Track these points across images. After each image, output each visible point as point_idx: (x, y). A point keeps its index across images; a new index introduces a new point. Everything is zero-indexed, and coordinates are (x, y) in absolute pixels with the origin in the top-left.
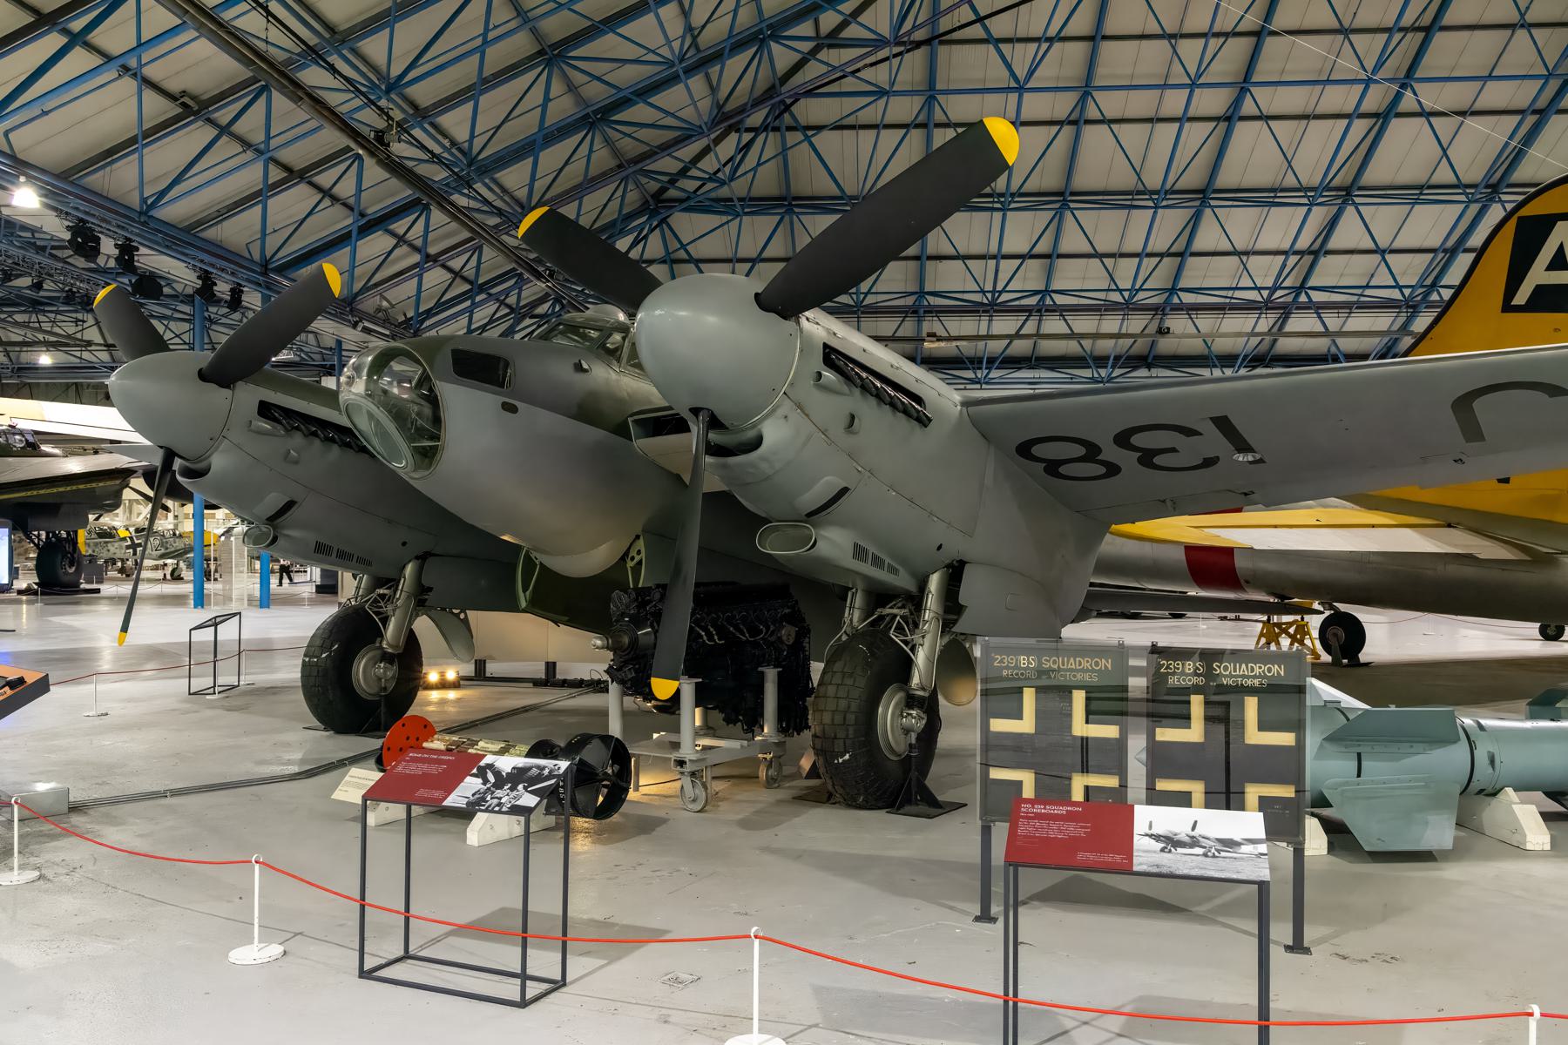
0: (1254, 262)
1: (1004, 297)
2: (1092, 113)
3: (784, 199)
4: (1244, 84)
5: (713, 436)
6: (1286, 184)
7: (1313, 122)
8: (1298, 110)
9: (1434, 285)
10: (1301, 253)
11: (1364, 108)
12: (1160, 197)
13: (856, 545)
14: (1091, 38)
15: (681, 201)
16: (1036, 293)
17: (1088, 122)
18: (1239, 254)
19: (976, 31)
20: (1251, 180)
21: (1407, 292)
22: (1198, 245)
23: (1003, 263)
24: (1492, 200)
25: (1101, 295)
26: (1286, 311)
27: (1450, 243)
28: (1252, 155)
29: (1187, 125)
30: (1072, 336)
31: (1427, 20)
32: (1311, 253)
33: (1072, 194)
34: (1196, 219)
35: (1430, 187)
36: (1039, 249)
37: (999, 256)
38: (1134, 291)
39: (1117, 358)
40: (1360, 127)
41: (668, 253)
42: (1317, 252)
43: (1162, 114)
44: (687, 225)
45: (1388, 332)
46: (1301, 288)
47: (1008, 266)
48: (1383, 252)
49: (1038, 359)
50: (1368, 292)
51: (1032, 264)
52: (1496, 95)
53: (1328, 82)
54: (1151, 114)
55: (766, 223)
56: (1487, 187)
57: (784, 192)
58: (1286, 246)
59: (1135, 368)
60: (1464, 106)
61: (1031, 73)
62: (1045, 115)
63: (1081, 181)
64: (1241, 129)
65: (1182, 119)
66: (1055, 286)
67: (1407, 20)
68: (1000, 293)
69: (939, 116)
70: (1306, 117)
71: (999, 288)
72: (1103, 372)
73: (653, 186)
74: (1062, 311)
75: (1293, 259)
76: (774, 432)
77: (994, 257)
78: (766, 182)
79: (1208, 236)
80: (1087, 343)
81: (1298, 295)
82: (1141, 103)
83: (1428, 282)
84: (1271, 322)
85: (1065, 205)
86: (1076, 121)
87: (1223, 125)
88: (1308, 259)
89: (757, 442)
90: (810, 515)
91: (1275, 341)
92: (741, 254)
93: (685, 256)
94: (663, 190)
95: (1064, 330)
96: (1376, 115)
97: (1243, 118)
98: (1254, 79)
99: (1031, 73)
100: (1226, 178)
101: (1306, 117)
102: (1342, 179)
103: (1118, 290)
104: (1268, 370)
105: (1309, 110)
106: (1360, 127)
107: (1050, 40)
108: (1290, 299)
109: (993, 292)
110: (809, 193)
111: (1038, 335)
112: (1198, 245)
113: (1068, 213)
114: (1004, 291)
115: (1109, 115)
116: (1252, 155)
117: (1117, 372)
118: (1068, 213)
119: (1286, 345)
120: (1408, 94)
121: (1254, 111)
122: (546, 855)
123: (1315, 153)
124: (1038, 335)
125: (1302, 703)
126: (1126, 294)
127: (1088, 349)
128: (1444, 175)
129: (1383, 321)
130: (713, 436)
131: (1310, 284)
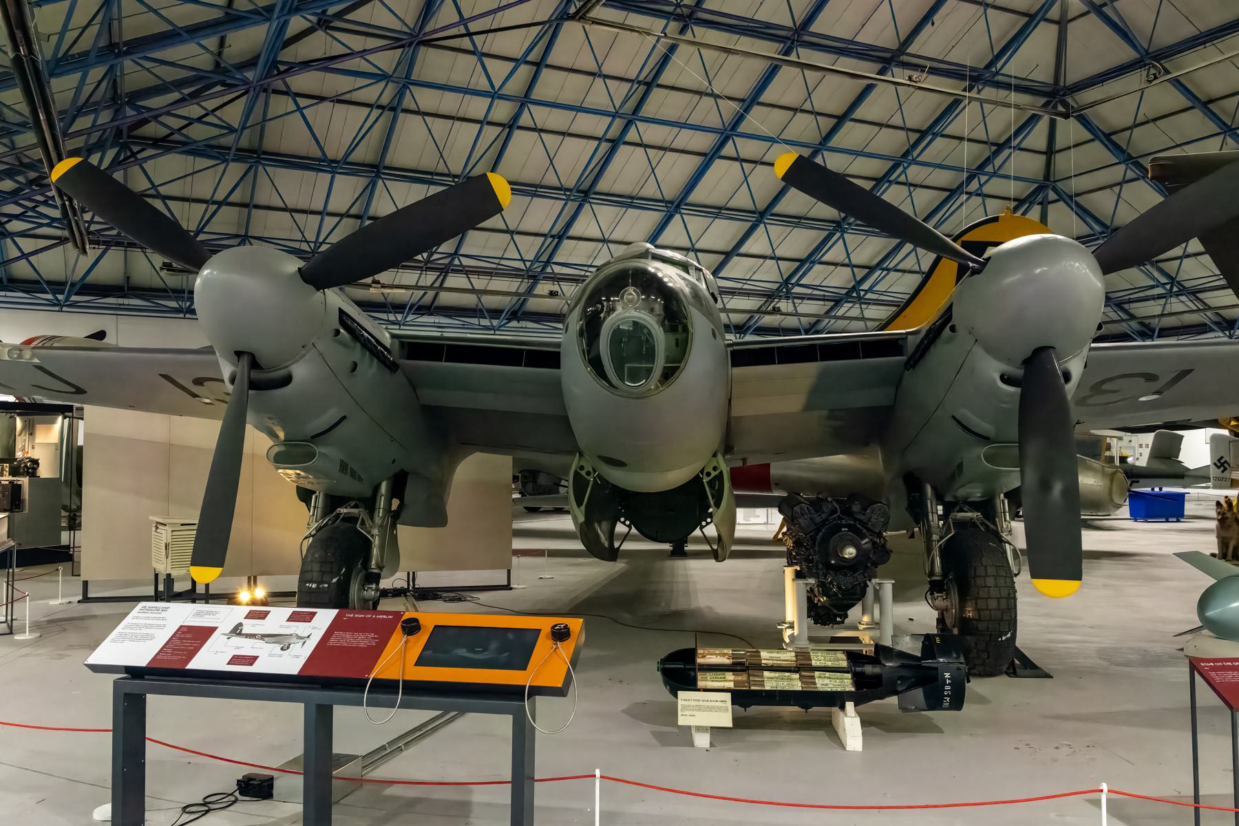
3: (254, 152)
4: (729, 132)
5: (255, 375)
7: (567, 139)
8: (659, 143)
13: (342, 461)
15: (184, 144)
18: (512, 233)
19: (466, 43)
20: (617, 189)
23: (327, 219)
24: (584, 201)
26: (535, 278)
29: (486, 127)
30: (473, 291)
31: (649, 79)
34: (372, 186)
35: (542, 187)
39: (412, 306)
40: (491, 133)
45: (516, 294)
47: (330, 222)
48: (512, 233)
50: (503, 262)
54: (564, 129)
60: (757, 158)
65: (484, 122)
67: (641, 78)
68: (321, 244)
70: (563, 134)
74: (467, 272)
76: (300, 371)
81: (453, 260)
82: (449, 102)
83: (544, 258)
85: (378, 176)
87: (388, 115)
89: (288, 380)
90: (313, 437)
91: (437, 294)
95: (791, 309)
97: (1050, 203)
101: (563, 134)
102: (585, 186)
104: (121, 301)
105: (667, 145)
106: (491, 133)
108: (446, 261)
109: (315, 243)
110: (275, 150)
113: (261, 168)
115: (646, 141)
118: (261, 168)
119: (446, 298)
120: (633, 128)
122: (704, 680)
128: (551, 180)
130: (255, 375)
131: (461, 252)
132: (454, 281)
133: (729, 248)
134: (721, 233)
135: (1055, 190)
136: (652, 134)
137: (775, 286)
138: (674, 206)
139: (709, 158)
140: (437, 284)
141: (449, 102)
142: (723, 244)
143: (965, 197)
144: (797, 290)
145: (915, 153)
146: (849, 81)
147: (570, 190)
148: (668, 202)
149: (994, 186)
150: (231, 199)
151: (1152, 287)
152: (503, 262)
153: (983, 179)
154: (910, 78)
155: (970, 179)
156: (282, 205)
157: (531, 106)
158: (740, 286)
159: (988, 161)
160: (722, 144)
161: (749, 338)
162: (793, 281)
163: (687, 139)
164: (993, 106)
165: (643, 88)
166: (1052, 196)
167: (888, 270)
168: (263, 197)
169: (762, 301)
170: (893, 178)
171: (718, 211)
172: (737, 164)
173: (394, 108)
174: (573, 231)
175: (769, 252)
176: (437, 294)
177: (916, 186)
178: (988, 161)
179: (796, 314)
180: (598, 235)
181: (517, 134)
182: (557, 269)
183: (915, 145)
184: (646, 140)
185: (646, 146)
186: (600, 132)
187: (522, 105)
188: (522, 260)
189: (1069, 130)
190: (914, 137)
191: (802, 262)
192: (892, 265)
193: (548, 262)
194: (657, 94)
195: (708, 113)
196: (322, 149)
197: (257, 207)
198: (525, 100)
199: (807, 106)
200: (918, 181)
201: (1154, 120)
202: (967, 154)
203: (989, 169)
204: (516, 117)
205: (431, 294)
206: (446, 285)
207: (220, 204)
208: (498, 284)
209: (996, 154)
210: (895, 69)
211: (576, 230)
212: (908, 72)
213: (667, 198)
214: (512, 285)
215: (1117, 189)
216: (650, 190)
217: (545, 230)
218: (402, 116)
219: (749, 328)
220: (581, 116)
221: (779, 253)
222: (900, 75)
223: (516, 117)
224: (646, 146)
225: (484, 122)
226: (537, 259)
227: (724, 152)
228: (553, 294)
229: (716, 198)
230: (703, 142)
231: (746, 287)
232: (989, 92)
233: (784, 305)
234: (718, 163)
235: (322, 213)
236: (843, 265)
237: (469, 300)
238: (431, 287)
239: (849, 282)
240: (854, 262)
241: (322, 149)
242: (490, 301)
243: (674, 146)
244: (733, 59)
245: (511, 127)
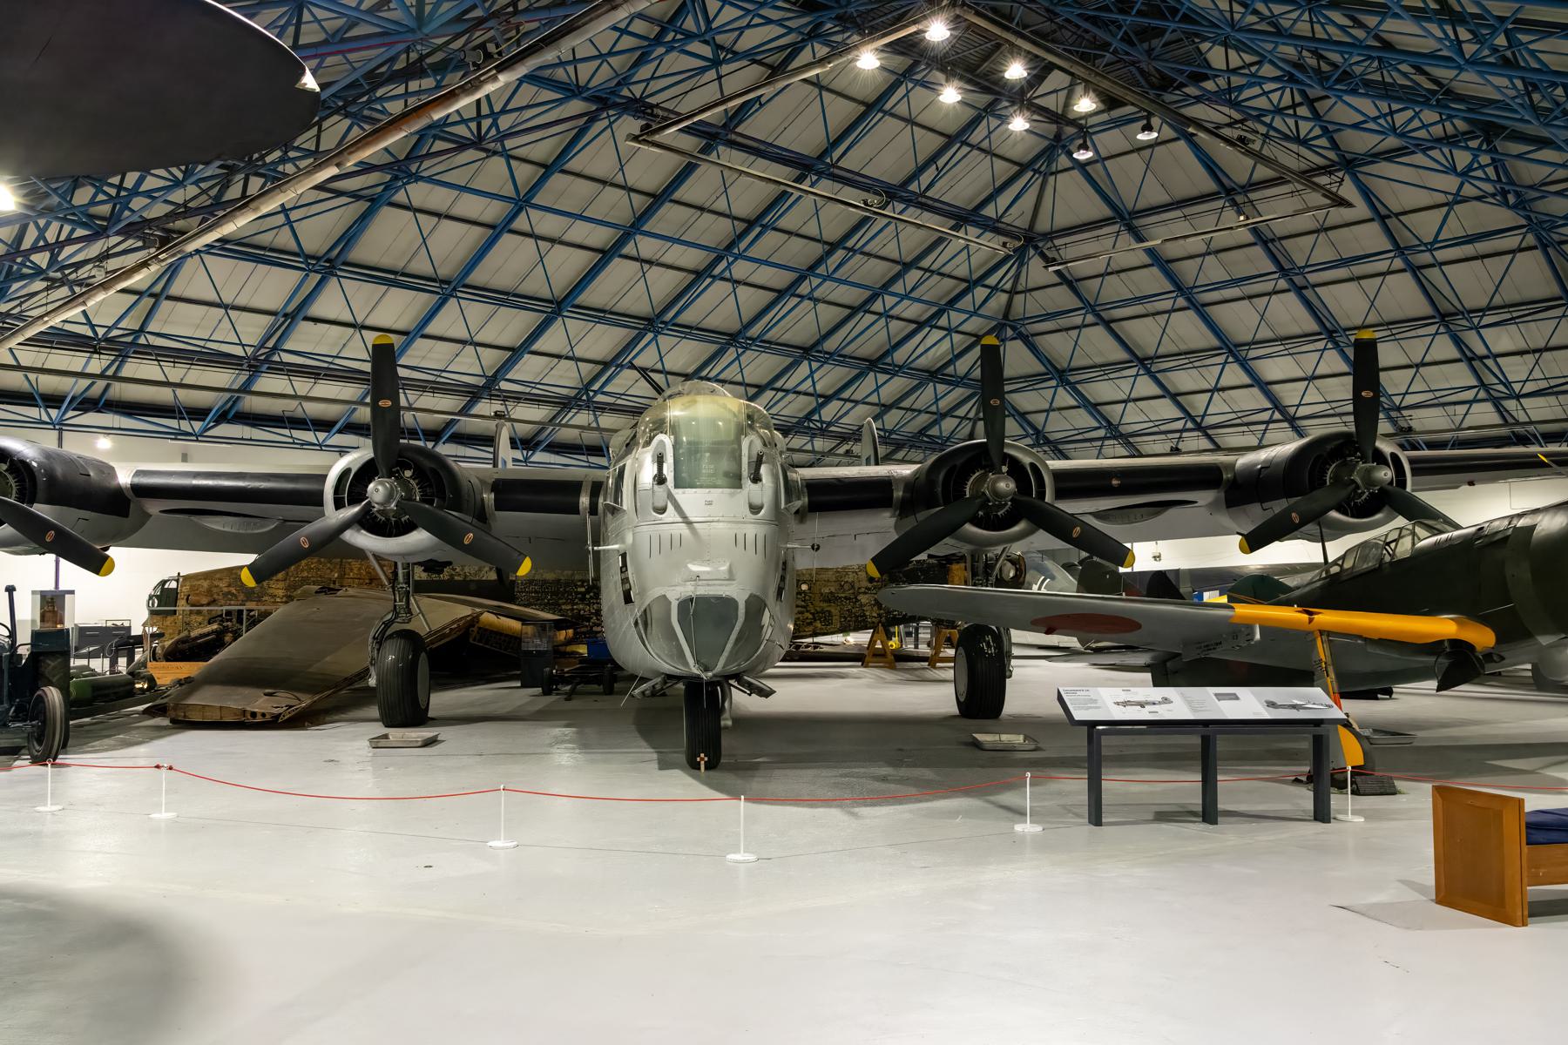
18: (226, 307)
21: (250, 351)
22: (175, 290)
25: (201, 343)
27: (290, 309)
32: (152, 295)
38: (830, 424)
48: (226, 307)
50: (337, 361)
52: (471, 206)
53: (581, 217)
54: (443, 208)
59: (86, 411)
61: (913, 289)
62: (473, 215)
72: (54, 413)
74: (160, 354)
81: (137, 338)
83: (270, 344)
84: (105, 363)
88: (147, 302)
91: (108, 386)
96: (492, 227)
98: (645, 228)
99: (913, 289)
107: (933, 272)
108: (129, 339)
117: (71, 413)
119: (252, 404)
121: (527, 228)
123: (450, 245)
125: (1339, 676)
129: (538, 413)
131: (286, 347)
132: (132, 368)
133: (764, 382)
134: (509, 325)
135: (1014, 328)
136: (547, 224)
137: (573, 393)
138: (557, 307)
139: (497, 230)
142: (511, 337)
143: (709, 280)
144: (600, 398)
145: (743, 245)
146: (772, 186)
148: (442, 282)
149: (828, 290)
151: (1096, 429)
152: (337, 361)
153: (890, 300)
154: (865, 203)
155: (718, 259)
158: (528, 390)
159: (820, 261)
160: (513, 217)
161: (539, 456)
162: (596, 387)
164: (1259, 336)
166: (1010, 332)
167: (787, 391)
170: (717, 271)
171: (601, 315)
175: (565, 351)
176: (108, 386)
177: (650, 262)
178: (820, 261)
179: (598, 429)
180: (464, 335)
182: (287, 358)
183: (741, 236)
185: (537, 237)
188: (93, 327)
189: (1036, 271)
190: (740, 226)
191: (606, 365)
192: (712, 375)
193: (275, 349)
194: (557, 181)
199: (619, 179)
201: (1118, 272)
202: (800, 252)
203: (821, 270)
205: (101, 384)
208: (197, 375)
209: (829, 253)
210: (721, 148)
211: (316, 309)
212: (1003, 239)
213: (443, 272)
214: (222, 377)
215: (1074, 333)
216: (421, 266)
219: (538, 444)
220: (468, 198)
221: (578, 352)
222: (727, 155)
224: (537, 237)
227: (516, 225)
229: (503, 281)
230: (600, 236)
231: (619, 402)
232: (825, 187)
233: (583, 418)
234: (507, 240)
236: (567, 358)
238: (102, 376)
240: (668, 367)
242: (48, 383)
243: (663, 260)
244: (744, 178)
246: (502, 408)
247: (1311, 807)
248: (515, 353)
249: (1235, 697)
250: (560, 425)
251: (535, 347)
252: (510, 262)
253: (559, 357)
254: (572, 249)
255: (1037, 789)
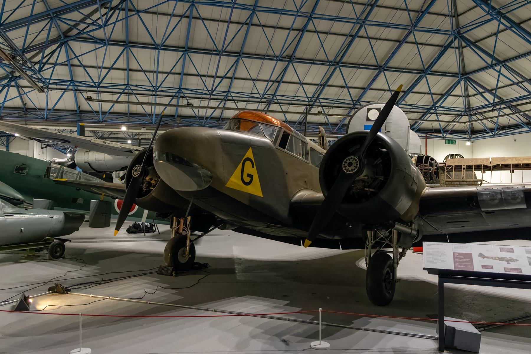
0: (258, 83)
1: (215, 93)
2: (255, 21)
3: (125, 42)
6: (319, 57)
7: (329, 35)
9: (215, 90)
10: (273, 81)
11: (295, 26)
12: (221, 53)
14: (458, 16)
16: (226, 92)
17: (252, 25)
22: (285, 79)
23: (217, 79)
25: (249, 95)
28: (310, 45)
32: (277, 82)
33: (189, 48)
34: (237, 62)
36: (228, 75)
37: (157, 72)
41: (68, 60)
42: (323, 85)
43: (280, 25)
44: (78, 47)
46: (274, 95)
47: (161, 77)
49: (222, 119)
50: (295, 98)
51: (461, 98)
54: (274, 24)
55: (116, 50)
56: (335, 62)
57: (124, 39)
58: (268, 78)
63: (246, 50)
64: (307, 36)
66: (232, 90)
69: (195, 14)
71: (158, 86)
73: (65, 27)
75: (270, 83)
77: (155, 72)
78: (118, 33)
79: (290, 76)
80: (196, 110)
83: (316, 96)
86: (248, 24)
92: (105, 65)
93: (78, 63)
94: (70, 30)
100: (298, 54)
103: (259, 94)
108: (271, 97)
111: (178, 106)
112: (285, 79)
114: (265, 94)
115: (318, 29)
116: (257, 39)
120: (412, 35)
123: (280, 41)
124: (178, 106)
126: (309, 99)
127: (197, 114)
128: (270, 53)
134: (316, 74)
136: (372, 31)
140: (266, 109)
141: (272, 19)
147: (278, 57)
150: (228, 76)
156: (197, 73)
157: (257, 12)
163: (338, 27)
165: (370, 7)
168: (134, 65)
169: (454, 117)
172: (316, 34)
173: (303, 30)
174: (330, 83)
180: (297, 80)
181: (306, 34)
184: (318, 29)
186: (289, 25)
187: (309, 19)
191: (442, 95)
195: (403, 18)
196: (407, 6)
197: (179, 74)
198: (310, 17)
200: (423, 41)
204: (306, 25)
206: (270, 109)
207: (110, 69)
213: (331, 58)
217: (318, 82)
218: (137, 15)
223: (306, 25)
225: (229, 22)
226: (313, 97)
228: (319, 113)
235: (157, 72)
237: (436, 125)
239: (431, 103)
241: (407, 6)
245: (303, 31)
246: (322, 110)
247: (482, 339)
248: (323, 85)
249: (483, 267)
250: (423, 120)
251: (414, 90)
252: (360, 50)
253: (424, 93)
254: (336, 36)
255: (78, 321)
